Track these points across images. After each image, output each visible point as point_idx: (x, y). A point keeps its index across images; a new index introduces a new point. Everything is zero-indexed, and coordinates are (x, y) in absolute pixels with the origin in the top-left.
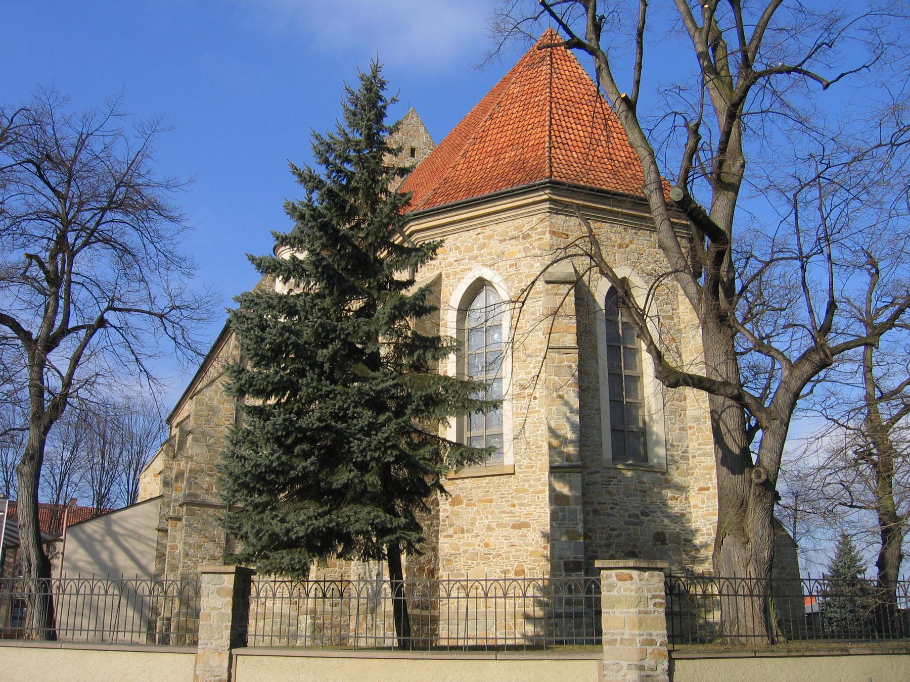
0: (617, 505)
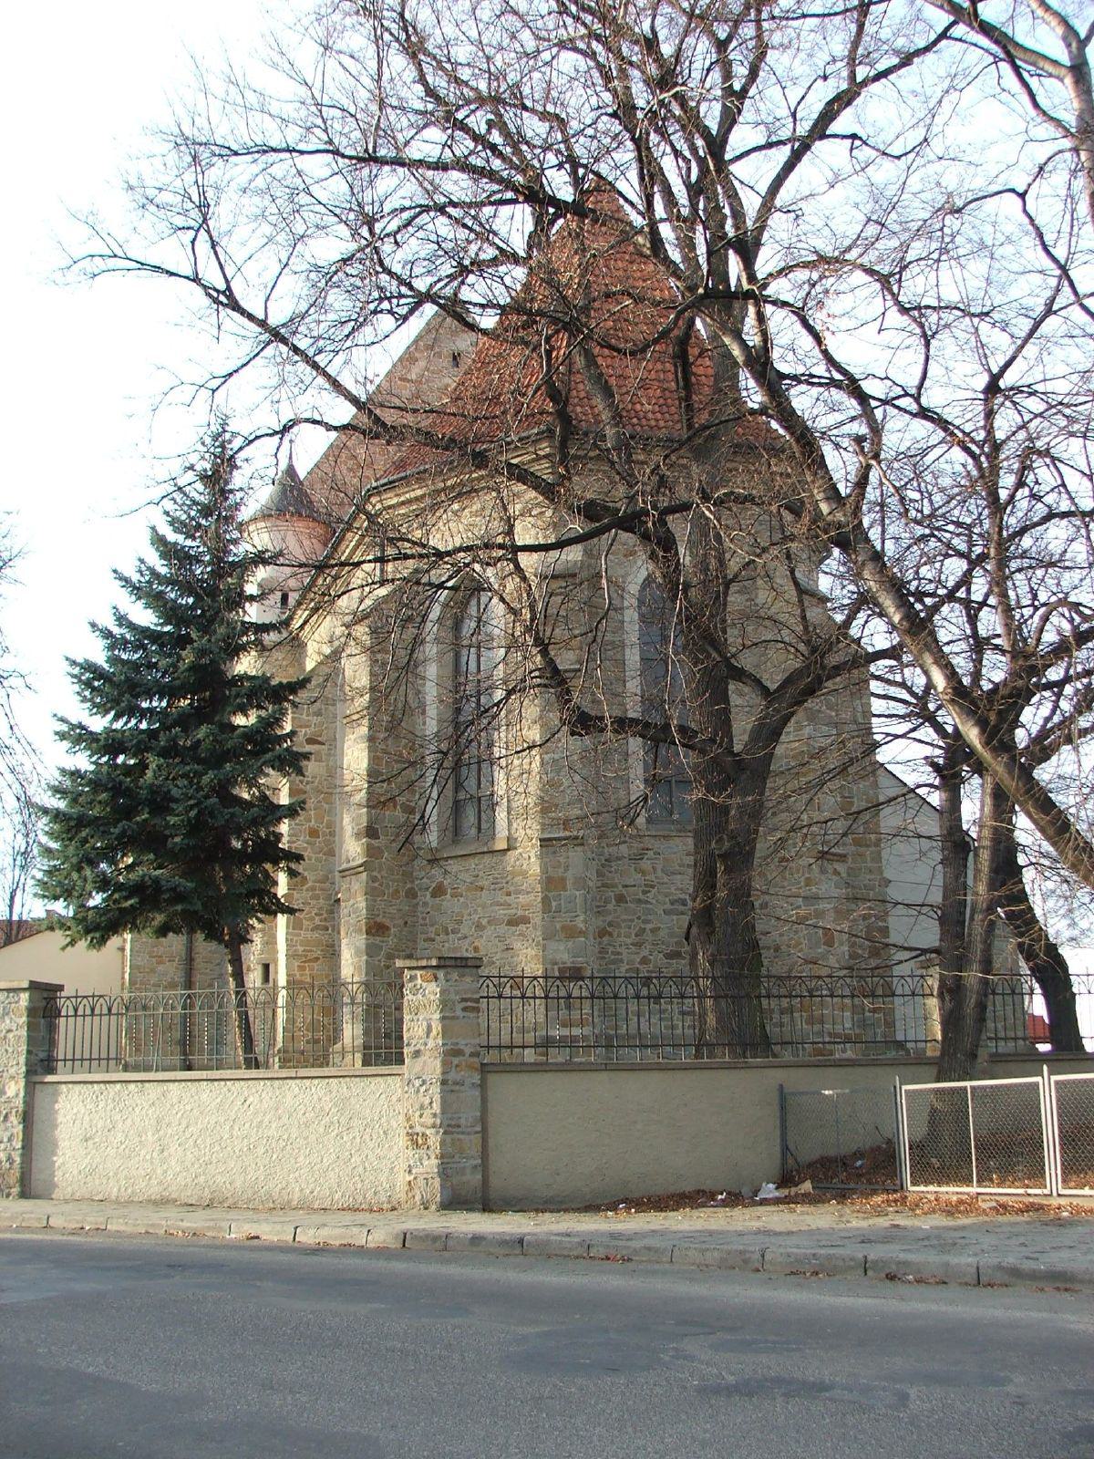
0: (653, 887)
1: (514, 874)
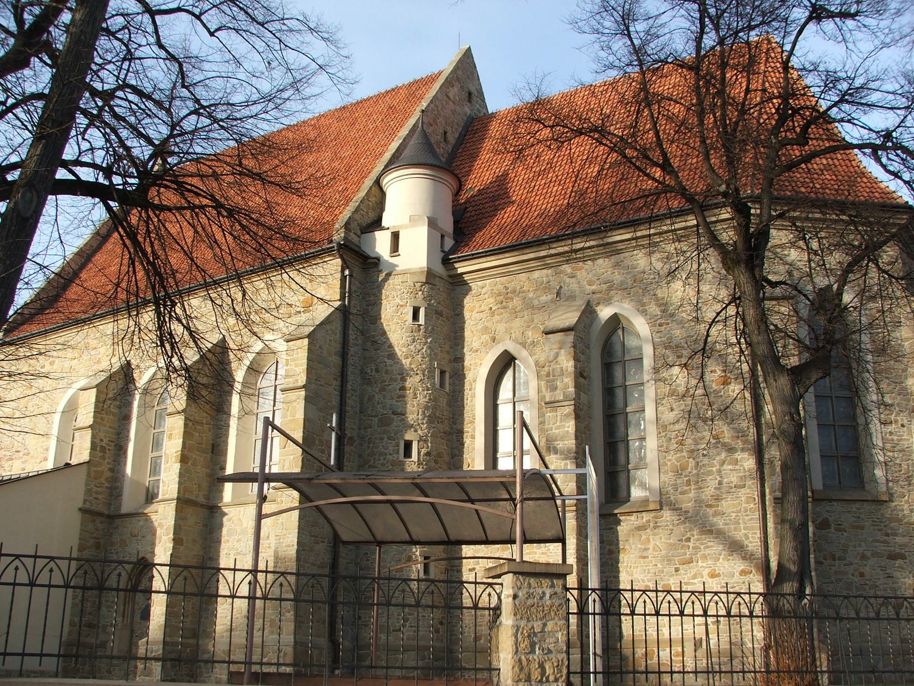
1: (891, 520)
